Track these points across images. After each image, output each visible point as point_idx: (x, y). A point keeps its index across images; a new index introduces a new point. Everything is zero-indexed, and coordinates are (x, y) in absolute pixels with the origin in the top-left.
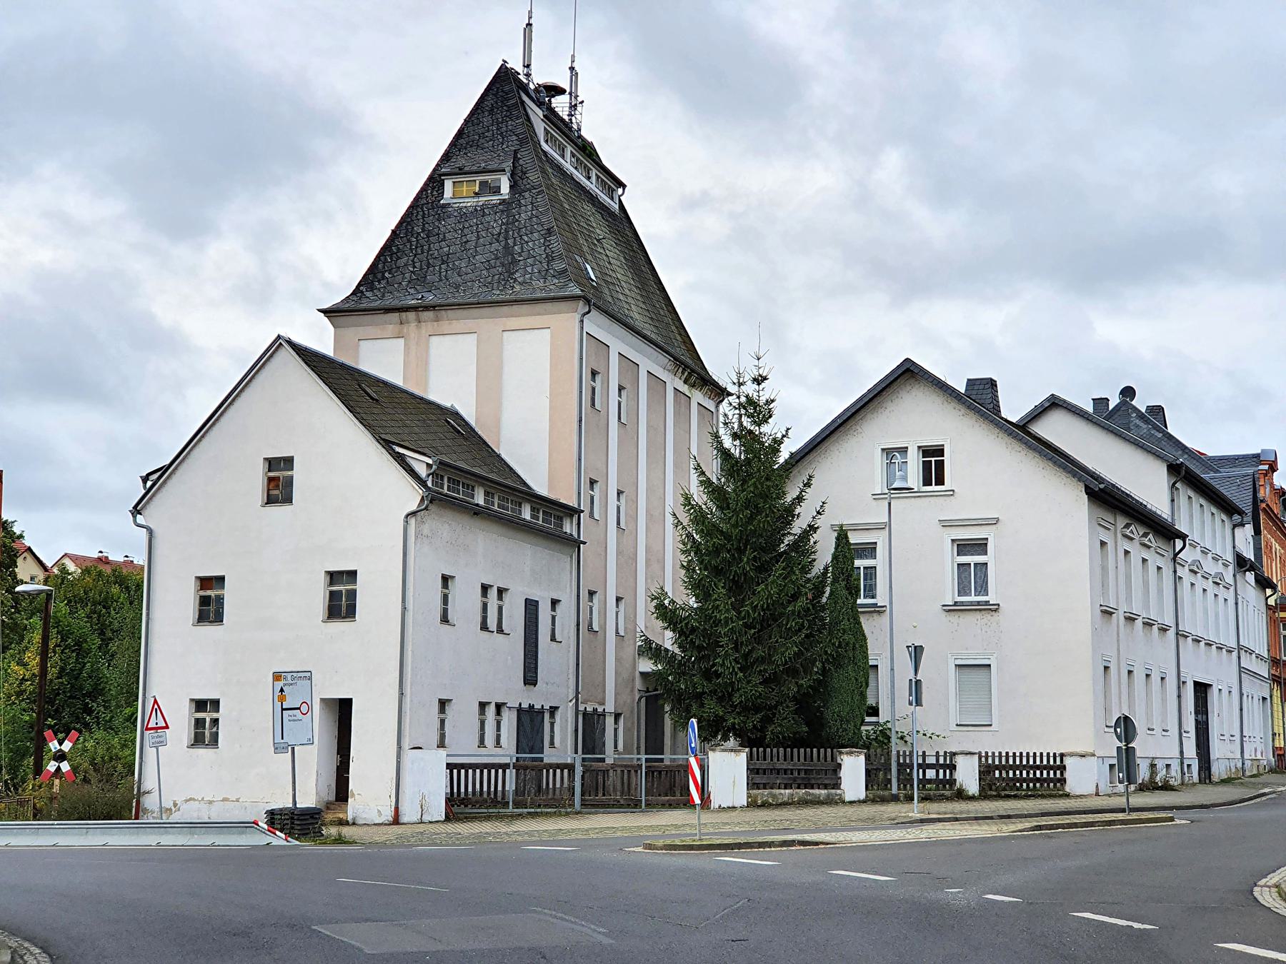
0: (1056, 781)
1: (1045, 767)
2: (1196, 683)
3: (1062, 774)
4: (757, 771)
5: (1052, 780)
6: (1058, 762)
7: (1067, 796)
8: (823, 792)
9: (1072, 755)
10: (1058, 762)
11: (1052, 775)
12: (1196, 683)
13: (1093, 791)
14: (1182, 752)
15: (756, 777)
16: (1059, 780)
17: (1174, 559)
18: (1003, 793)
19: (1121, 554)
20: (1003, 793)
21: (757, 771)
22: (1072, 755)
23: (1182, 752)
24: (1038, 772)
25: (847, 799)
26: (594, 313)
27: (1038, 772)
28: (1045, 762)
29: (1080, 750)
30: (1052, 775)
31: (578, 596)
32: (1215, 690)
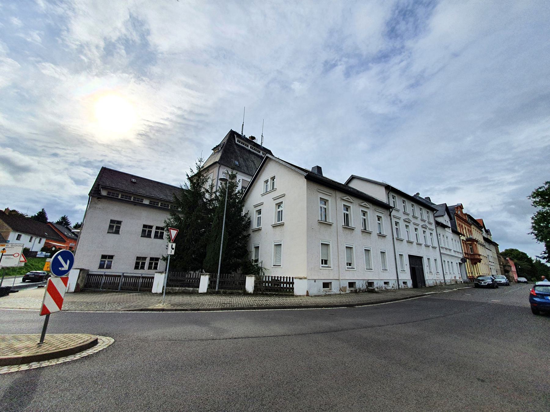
0: (290, 288)
1: (285, 283)
2: (410, 257)
3: (293, 286)
4: (170, 280)
5: (288, 288)
6: (291, 281)
7: (297, 296)
8: (191, 289)
9: (295, 278)
10: (291, 281)
11: (288, 286)
12: (410, 257)
13: (305, 293)
14: (398, 278)
15: (170, 283)
16: (291, 288)
17: (390, 215)
18: (264, 293)
19: (394, 224)
20: (264, 293)
21: (170, 280)
22: (295, 278)
23: (398, 278)
24: (285, 285)
25: (200, 292)
26: (222, 166)
27: (285, 285)
28: (285, 281)
29: (302, 276)
30: (288, 286)
31: (396, 259)
32: (425, 261)
